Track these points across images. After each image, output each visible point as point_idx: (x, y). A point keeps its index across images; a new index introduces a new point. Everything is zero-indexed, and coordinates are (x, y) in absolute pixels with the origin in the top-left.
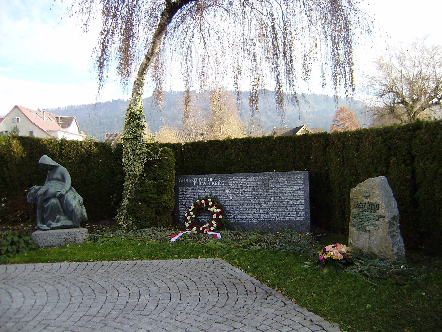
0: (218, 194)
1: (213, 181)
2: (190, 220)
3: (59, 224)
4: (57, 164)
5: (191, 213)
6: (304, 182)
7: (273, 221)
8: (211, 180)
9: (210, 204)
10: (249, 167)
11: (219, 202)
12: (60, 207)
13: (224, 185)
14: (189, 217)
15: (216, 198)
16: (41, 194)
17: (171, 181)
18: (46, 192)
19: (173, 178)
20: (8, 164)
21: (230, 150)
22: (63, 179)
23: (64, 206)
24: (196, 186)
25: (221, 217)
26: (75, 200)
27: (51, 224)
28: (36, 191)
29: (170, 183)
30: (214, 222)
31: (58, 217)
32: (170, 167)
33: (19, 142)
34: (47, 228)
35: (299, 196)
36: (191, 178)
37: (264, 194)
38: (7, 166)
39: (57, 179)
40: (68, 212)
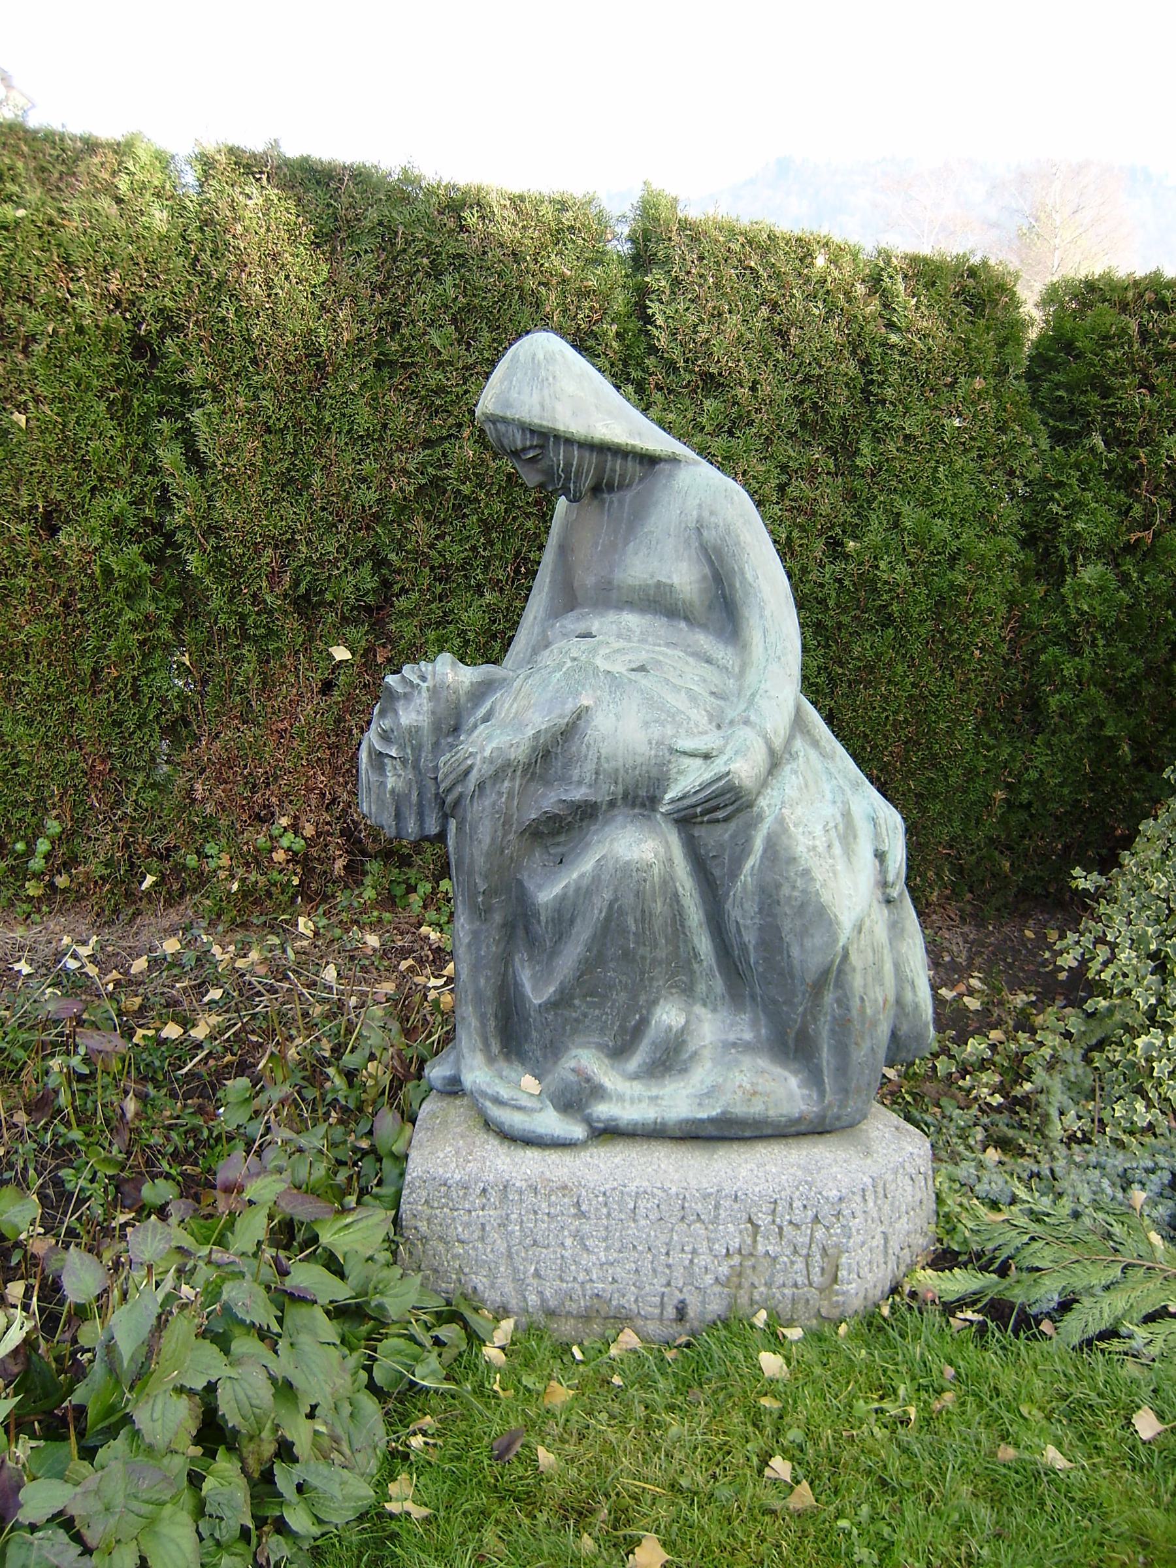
3: (678, 1100)
4: (651, 437)
12: (695, 914)
16: (502, 770)
18: (552, 753)
20: (196, 416)
22: (721, 607)
23: (743, 913)
26: (840, 839)
27: (597, 1092)
28: (452, 723)
31: (669, 1015)
33: (286, 211)
34: (550, 1122)
38: (186, 435)
39: (659, 603)
40: (773, 976)
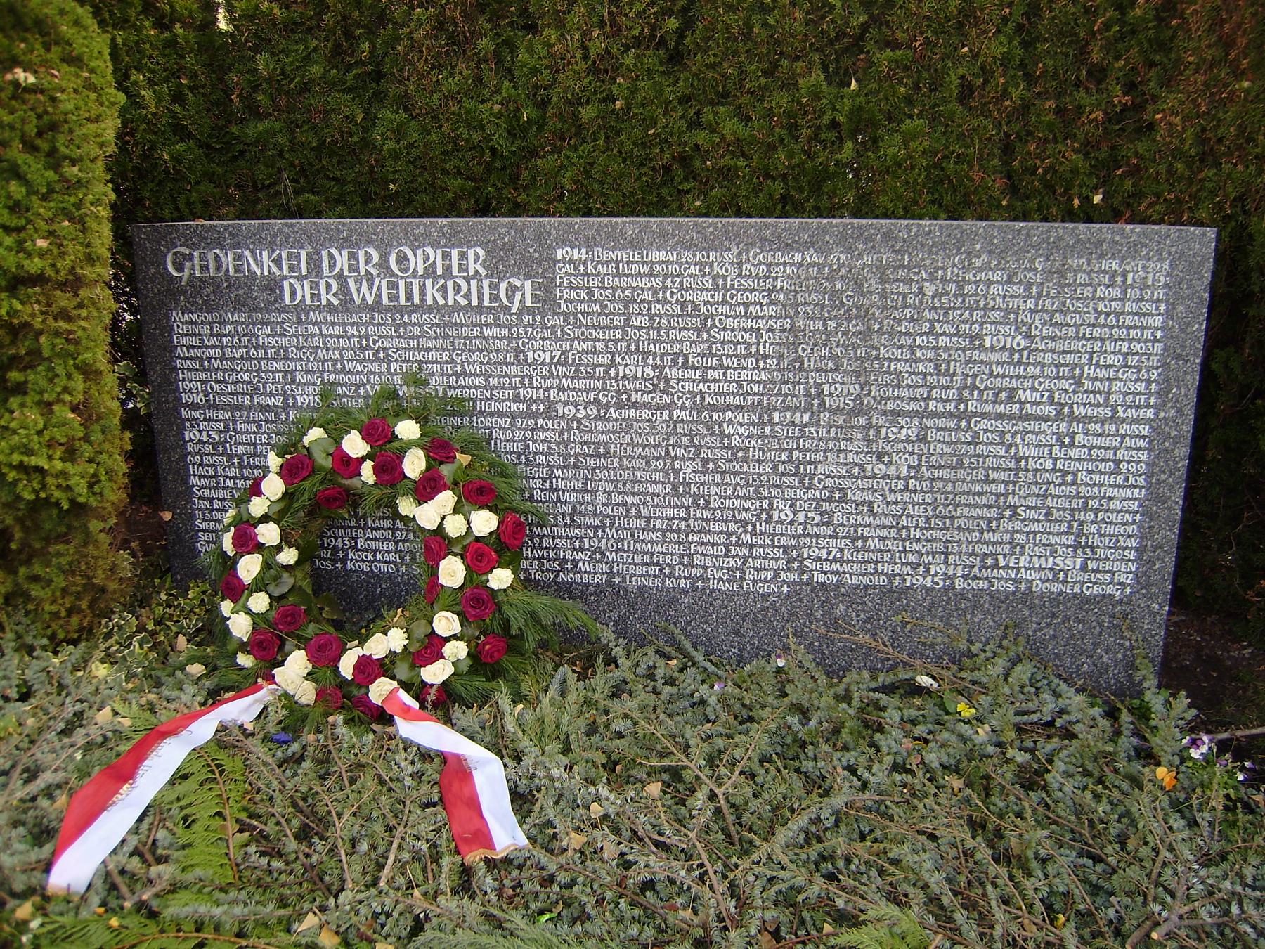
0: (469, 376)
1: (430, 272)
2: (259, 585)
5: (269, 534)
6: (1169, 314)
7: (894, 594)
8: (417, 261)
9: (414, 465)
10: (683, 160)
11: (478, 445)
13: (523, 310)
14: (249, 567)
15: (458, 407)
17: (74, 283)
19: (91, 259)
21: (551, 34)
24: (300, 309)
25: (500, 578)
29: (63, 300)
30: (446, 623)
32: (54, 160)
35: (1113, 419)
36: (257, 243)
37: (840, 390)
